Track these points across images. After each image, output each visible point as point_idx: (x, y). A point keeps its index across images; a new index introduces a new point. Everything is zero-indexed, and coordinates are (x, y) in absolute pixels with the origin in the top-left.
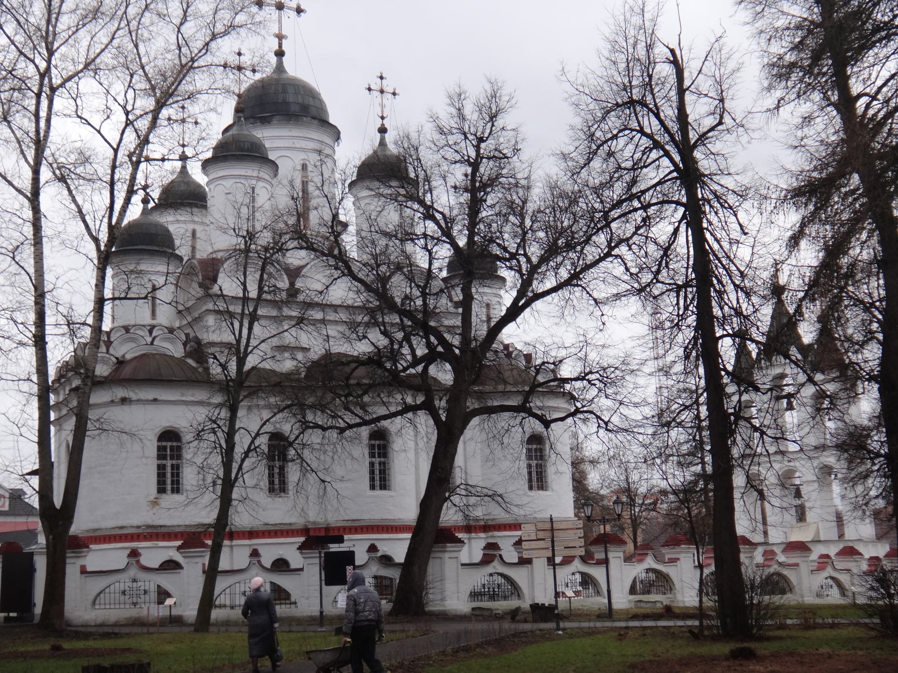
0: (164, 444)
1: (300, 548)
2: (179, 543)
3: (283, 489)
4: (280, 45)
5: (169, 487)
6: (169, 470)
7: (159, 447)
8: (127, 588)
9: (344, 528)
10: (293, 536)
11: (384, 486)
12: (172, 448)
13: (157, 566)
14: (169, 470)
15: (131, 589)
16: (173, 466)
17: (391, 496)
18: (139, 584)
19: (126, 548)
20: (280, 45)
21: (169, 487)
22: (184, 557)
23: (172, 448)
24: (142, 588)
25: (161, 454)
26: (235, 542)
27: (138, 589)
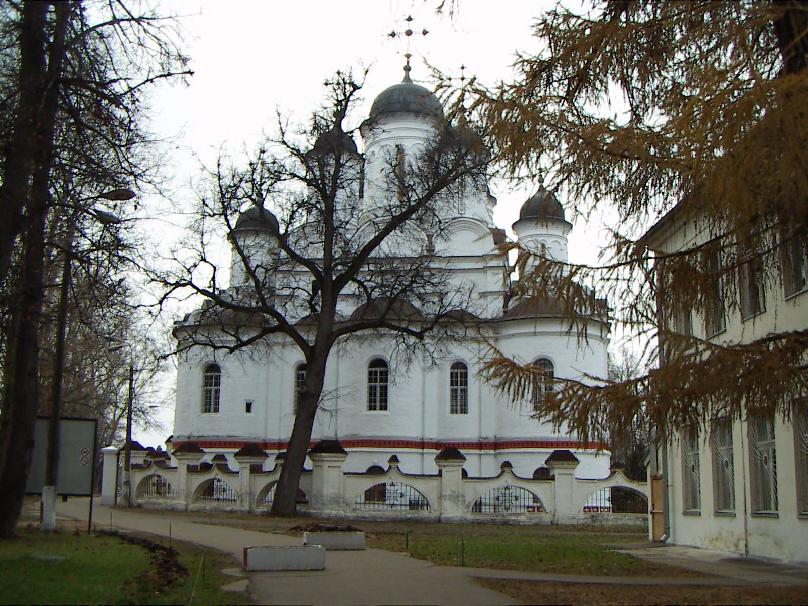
0: (374, 369)
1: (437, 458)
2: (237, 450)
3: (464, 410)
4: (408, 62)
5: (378, 405)
6: (378, 390)
7: (370, 373)
8: (501, 495)
9: (458, 444)
10: (415, 448)
11: (384, 407)
12: (381, 373)
13: (364, 471)
14: (378, 390)
15: (504, 495)
16: (461, 390)
17: (385, 415)
18: (396, 488)
19: (213, 453)
20: (408, 62)
21: (378, 405)
22: (178, 459)
23: (381, 373)
24: (399, 491)
25: (372, 377)
26: (425, 451)
27: (510, 495)
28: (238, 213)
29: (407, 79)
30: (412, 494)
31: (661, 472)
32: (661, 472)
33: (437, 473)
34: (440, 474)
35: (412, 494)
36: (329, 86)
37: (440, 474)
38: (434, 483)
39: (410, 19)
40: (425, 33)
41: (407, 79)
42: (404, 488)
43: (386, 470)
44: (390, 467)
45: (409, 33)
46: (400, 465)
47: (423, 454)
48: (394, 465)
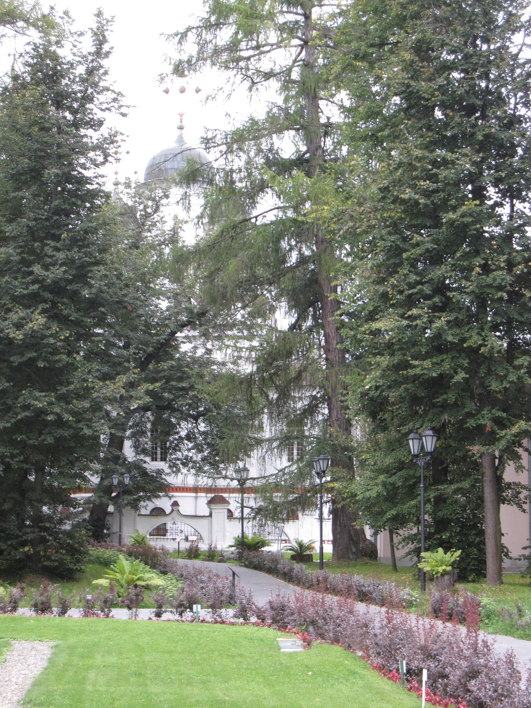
5: (159, 456)
21: (159, 456)
24: (179, 529)
26: (199, 494)
28: (238, 345)
29: (180, 140)
30: (189, 530)
31: (273, 428)
32: (273, 428)
33: (207, 514)
34: (211, 515)
35: (189, 530)
36: (217, 97)
37: (211, 515)
38: (206, 521)
39: (167, 91)
40: (128, 153)
41: (180, 140)
42: (183, 525)
43: (167, 512)
44: (173, 510)
45: (182, 91)
46: (180, 509)
47: (196, 497)
48: (175, 508)
